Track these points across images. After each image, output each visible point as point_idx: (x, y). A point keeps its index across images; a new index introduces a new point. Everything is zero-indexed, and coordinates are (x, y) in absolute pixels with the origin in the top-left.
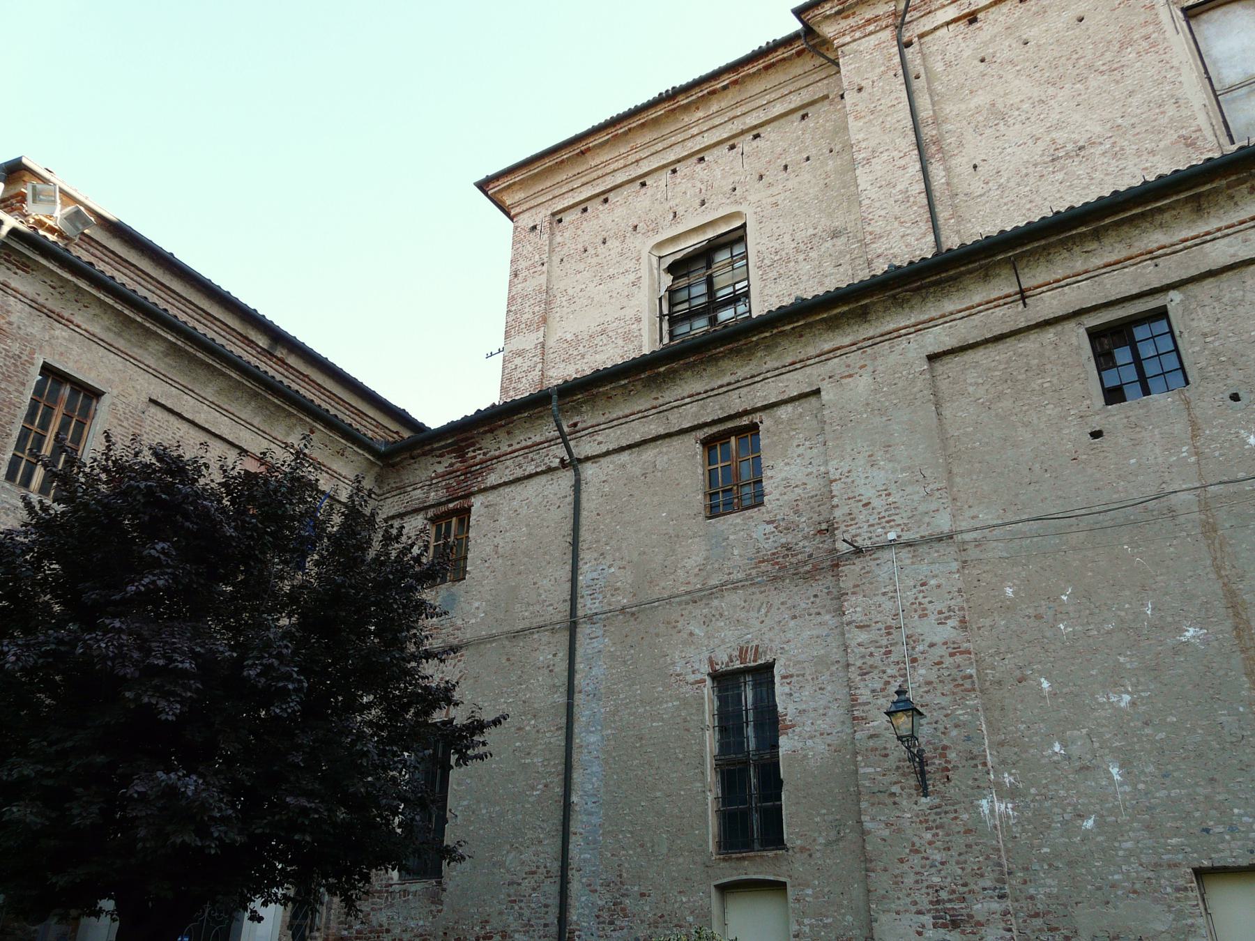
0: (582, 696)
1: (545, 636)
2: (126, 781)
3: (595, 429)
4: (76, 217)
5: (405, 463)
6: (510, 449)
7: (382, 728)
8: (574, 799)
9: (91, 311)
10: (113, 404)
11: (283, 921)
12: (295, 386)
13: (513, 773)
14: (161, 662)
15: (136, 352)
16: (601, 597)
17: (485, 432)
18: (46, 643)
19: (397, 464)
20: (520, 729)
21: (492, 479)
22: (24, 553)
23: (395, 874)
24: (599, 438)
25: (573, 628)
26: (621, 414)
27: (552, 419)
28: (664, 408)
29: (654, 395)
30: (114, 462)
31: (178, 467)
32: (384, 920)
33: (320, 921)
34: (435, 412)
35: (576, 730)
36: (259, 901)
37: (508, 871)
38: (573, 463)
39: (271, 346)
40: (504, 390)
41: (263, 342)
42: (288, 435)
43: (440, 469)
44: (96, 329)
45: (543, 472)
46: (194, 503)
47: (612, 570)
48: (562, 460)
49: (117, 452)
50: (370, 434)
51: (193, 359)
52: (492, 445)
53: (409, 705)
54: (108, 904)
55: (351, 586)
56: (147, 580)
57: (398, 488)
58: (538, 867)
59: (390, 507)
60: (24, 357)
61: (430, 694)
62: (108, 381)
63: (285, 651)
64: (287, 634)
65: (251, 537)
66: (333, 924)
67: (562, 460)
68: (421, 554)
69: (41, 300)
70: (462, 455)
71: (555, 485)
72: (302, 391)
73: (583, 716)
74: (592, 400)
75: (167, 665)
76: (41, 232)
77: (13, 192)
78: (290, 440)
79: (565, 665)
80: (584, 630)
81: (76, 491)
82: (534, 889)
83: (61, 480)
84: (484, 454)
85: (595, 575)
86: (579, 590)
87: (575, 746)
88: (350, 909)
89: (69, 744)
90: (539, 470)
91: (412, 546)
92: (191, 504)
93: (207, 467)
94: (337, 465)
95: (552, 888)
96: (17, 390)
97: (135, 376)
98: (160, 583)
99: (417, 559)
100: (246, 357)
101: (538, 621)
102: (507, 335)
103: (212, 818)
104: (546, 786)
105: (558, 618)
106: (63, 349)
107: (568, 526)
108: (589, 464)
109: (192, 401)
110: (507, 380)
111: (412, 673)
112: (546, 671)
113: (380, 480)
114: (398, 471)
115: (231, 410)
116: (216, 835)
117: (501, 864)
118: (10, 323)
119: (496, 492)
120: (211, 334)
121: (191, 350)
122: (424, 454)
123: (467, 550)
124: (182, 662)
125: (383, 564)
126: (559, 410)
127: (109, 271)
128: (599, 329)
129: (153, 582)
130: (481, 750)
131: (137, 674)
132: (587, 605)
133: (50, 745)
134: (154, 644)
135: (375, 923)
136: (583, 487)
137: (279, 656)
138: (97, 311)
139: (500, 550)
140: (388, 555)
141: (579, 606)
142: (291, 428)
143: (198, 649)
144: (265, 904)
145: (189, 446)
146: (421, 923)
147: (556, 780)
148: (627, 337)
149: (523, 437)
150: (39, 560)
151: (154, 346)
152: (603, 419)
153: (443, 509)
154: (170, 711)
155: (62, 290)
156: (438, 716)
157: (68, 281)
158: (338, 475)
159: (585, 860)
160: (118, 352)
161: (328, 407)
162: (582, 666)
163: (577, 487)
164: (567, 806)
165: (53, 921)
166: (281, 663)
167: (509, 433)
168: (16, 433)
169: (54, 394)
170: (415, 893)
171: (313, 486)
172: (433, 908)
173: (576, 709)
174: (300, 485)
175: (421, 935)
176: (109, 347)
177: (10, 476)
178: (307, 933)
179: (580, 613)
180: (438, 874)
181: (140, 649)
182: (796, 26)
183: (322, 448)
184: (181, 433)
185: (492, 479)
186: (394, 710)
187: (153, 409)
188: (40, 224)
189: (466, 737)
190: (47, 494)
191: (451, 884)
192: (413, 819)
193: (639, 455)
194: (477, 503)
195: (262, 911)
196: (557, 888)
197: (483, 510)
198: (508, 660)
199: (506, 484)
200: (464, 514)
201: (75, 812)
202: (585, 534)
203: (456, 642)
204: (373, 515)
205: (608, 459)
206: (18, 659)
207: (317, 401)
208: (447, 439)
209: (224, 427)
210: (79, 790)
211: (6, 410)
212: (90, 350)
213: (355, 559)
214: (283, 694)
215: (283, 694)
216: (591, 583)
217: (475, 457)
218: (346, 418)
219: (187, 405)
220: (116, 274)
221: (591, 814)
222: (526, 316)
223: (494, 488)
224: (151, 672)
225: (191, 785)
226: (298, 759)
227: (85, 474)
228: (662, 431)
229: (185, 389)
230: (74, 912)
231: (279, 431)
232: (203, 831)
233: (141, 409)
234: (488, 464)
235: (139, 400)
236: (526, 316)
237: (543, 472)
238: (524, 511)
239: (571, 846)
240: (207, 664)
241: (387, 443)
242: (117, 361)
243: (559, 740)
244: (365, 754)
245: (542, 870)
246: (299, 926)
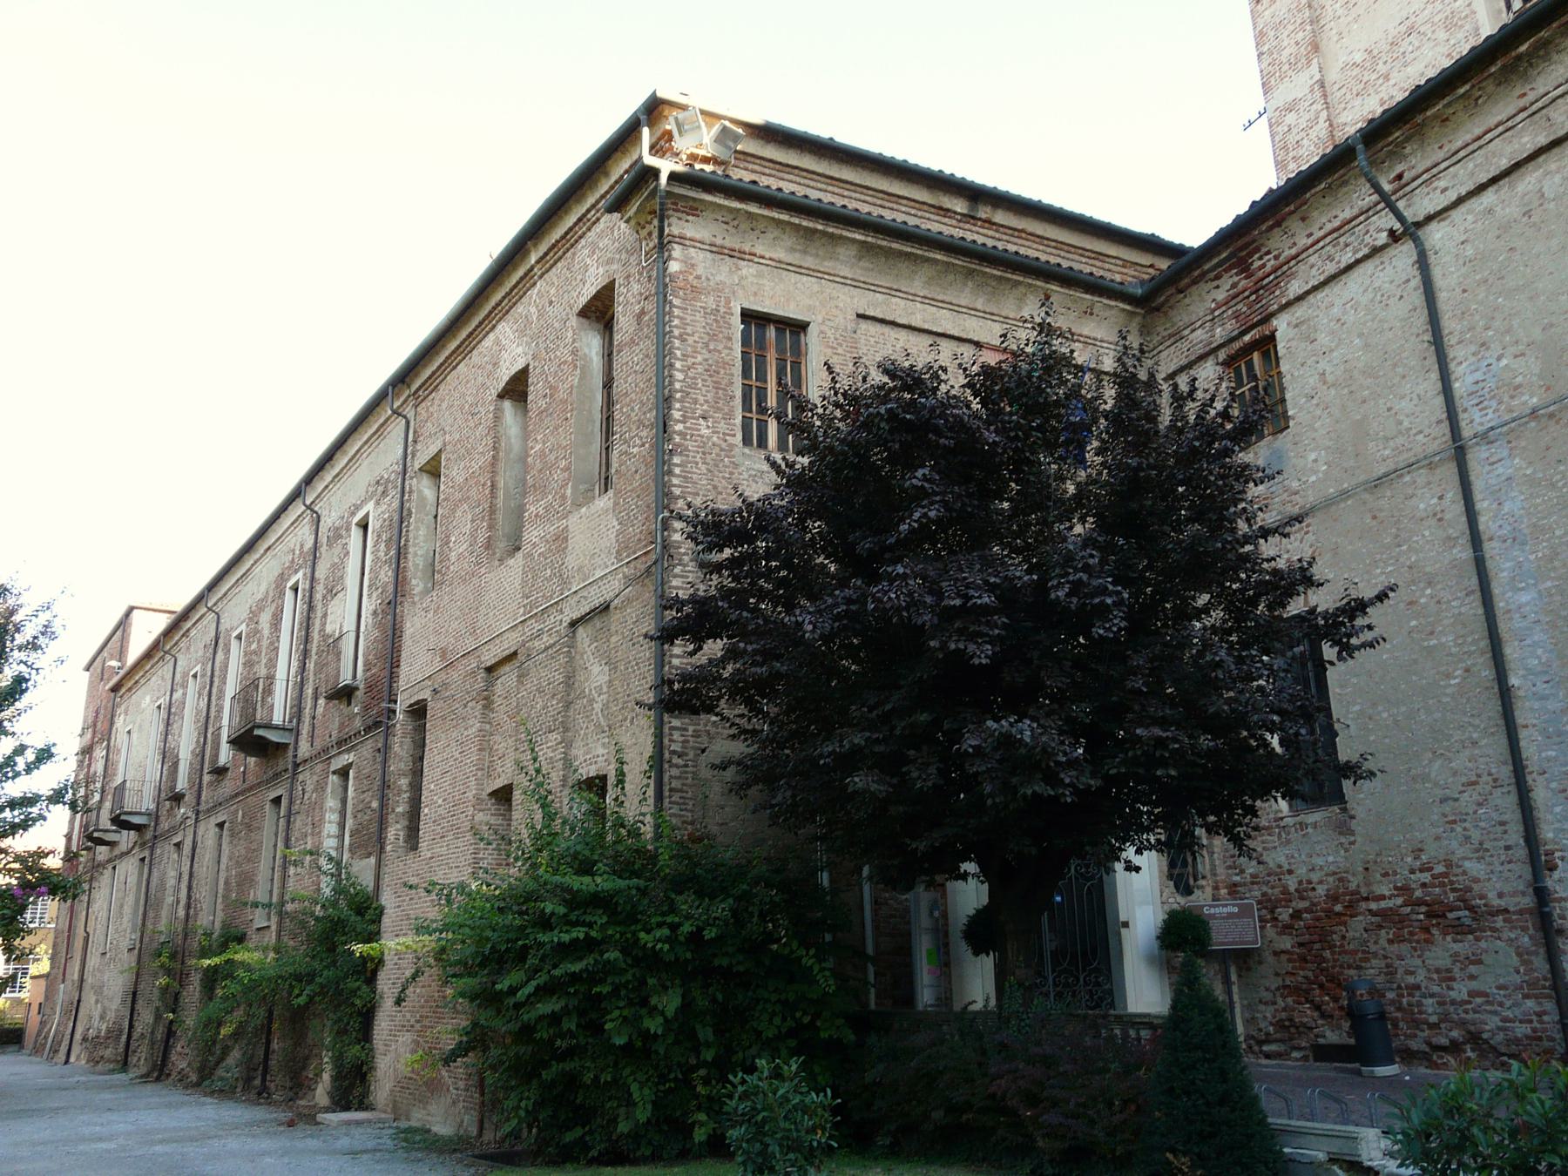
0: (1494, 544)
1: (1422, 476)
2: (955, 736)
3: (1432, 173)
4: (724, 136)
5: (1172, 301)
6: (1310, 241)
7: (1229, 632)
8: (1514, 681)
9: (770, 236)
11: (1161, 871)
12: (1012, 248)
13: (1415, 661)
14: (958, 602)
15: (828, 265)
16: (1494, 404)
17: (1271, 228)
18: (836, 605)
19: (1163, 304)
20: (1411, 603)
21: (1295, 288)
22: (786, 517)
23: (1283, 805)
24: (1442, 184)
25: (1460, 454)
26: (1468, 137)
27: (1363, 180)
28: (1539, 104)
29: (1518, 92)
30: (845, 395)
31: (914, 379)
32: (1282, 860)
33: (1204, 865)
34: (1192, 229)
35: (1496, 590)
36: (1132, 850)
37: (1436, 784)
38: (1409, 232)
39: (972, 208)
40: (1280, 165)
41: (960, 206)
42: (1020, 308)
43: (1221, 295)
44: (780, 254)
45: (1366, 257)
46: (943, 415)
47: (1504, 362)
48: (1392, 233)
49: (844, 383)
50: (1118, 278)
51: (889, 253)
52: (1281, 244)
53: (1257, 596)
54: (970, 867)
55: (1150, 467)
56: (917, 515)
57: (1170, 336)
58: (1479, 776)
59: (1169, 361)
60: (722, 310)
61: (1282, 578)
62: (810, 308)
63: (1091, 561)
64: (1088, 542)
65: (1017, 437)
66: (1220, 870)
67: (1392, 233)
68: (1228, 407)
69: (719, 241)
70: (1244, 267)
71: (1389, 269)
72: (1022, 251)
73: (1502, 569)
74: (1419, 133)
75: (964, 604)
76: (698, 166)
77: (658, 134)
78: (1026, 314)
79: (1460, 507)
80: (1477, 457)
81: (816, 436)
82: (1480, 804)
83: (795, 428)
84: (1276, 258)
85: (1478, 376)
86: (1458, 402)
87: (1499, 613)
88: (1240, 849)
89: (888, 707)
90: (1359, 255)
91: (1212, 400)
92: (940, 417)
93: (945, 370)
94: (1088, 328)
95: (1507, 802)
96: (726, 347)
97: (835, 294)
98: (932, 514)
99: (1225, 414)
100: (947, 231)
101: (1407, 457)
102: (1266, 88)
103: (1058, 763)
104: (1467, 670)
105: (1434, 446)
106: (754, 289)
107: (1422, 318)
108: (1434, 225)
109: (902, 303)
110: (1281, 150)
111: (1251, 561)
112: (1433, 522)
113: (1145, 330)
114: (1166, 314)
115: (948, 299)
116: (1067, 781)
117: (1425, 778)
118: (698, 277)
119: (1304, 304)
120: (900, 218)
121: (884, 243)
122: (1195, 282)
123: (1283, 390)
124: (980, 597)
125: (1181, 431)
126: (1372, 163)
127: (774, 184)
128: (1403, 28)
129: (925, 515)
130: (1368, 636)
131: (936, 621)
132: (1474, 421)
133: (870, 711)
134: (944, 584)
135: (1271, 865)
136: (1432, 259)
137: (1086, 568)
138: (776, 233)
139: (1330, 378)
140: (1184, 418)
141: (1463, 424)
142: (1021, 300)
143: (992, 580)
144: (1139, 852)
145: (919, 354)
146: (1331, 859)
147: (1481, 660)
148: (1450, 24)
149: (1325, 218)
150: (802, 520)
151: (845, 252)
152: (1441, 155)
153: (1237, 345)
154: (982, 654)
156: (1296, 607)
158: (1095, 339)
159: (1549, 759)
161: (1059, 260)
162: (1485, 504)
163: (1423, 263)
164: (1505, 694)
165: (921, 888)
166: (1090, 576)
167: (1303, 219)
168: (738, 393)
169: (762, 344)
170: (1315, 825)
171: (1066, 361)
172: (1343, 840)
173: (1489, 564)
174: (1054, 364)
175: (1335, 873)
176: (799, 270)
177: (747, 441)
178: (1191, 882)
179: (1467, 432)
180: (1339, 798)
181: (931, 592)
183: (1067, 312)
184: (901, 344)
185: (1295, 288)
186: (1239, 608)
187: (864, 326)
188: (693, 157)
189: (1343, 623)
190: (787, 450)
191: (1360, 809)
192: (1297, 734)
193: (1512, 187)
194: (1282, 326)
195: (1137, 860)
196: (1513, 799)
197: (1292, 333)
198: (1375, 517)
199: (1315, 289)
200: (1267, 344)
201: (915, 774)
202: (1449, 324)
203: (1296, 511)
204: (1152, 375)
205: (1463, 208)
206: (815, 627)
207: (1043, 258)
208: (1219, 253)
209: (945, 321)
210: (912, 752)
213: (1147, 432)
214: (1103, 612)
215: (1103, 612)
216: (1475, 388)
217: (1264, 266)
218: (1083, 266)
219: (897, 309)
220: (782, 184)
221: (1544, 698)
222: (1285, 53)
223: (1300, 298)
224: (948, 615)
225: (1026, 730)
226: (1138, 683)
227: (819, 416)
228: (1543, 140)
229: (891, 291)
230: (939, 878)
231: (1009, 308)
232: (1052, 779)
233: (863, 328)
234: (1283, 270)
235: (846, 319)
236: (1285, 53)
237: (1366, 257)
238: (1350, 317)
239: (1522, 744)
240: (1008, 595)
241: (1142, 282)
243: (1474, 608)
244: (1219, 665)
245: (1485, 778)
246: (1180, 875)
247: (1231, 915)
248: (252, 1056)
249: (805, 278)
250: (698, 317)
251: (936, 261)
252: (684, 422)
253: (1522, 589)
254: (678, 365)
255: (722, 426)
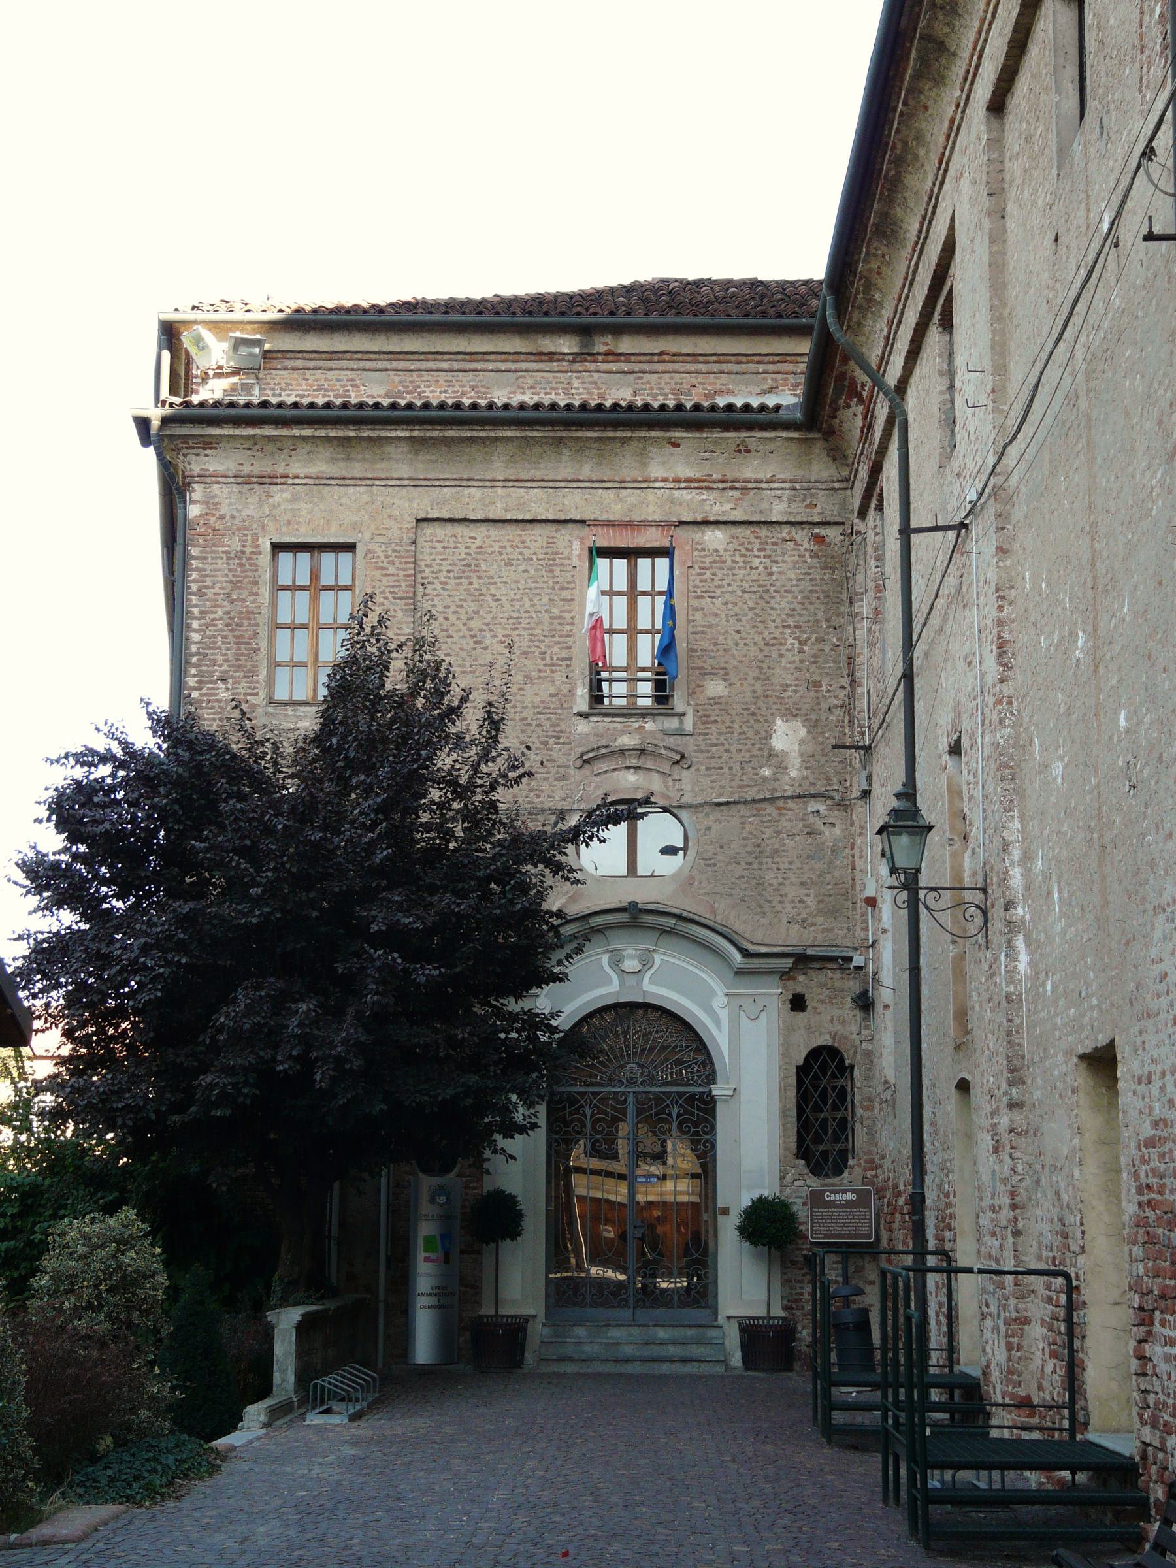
10: (369, 552)
15: (380, 469)
42: (645, 465)
60: (248, 550)
69: (246, 469)
98: (183, 961)
106: (289, 516)
118: (222, 517)
155: (258, 447)
157: (254, 436)
160: (357, 481)
176: (343, 481)
182: (151, 450)
184: (478, 542)
187: (429, 530)
211: (246, 623)
212: (322, 498)
219: (473, 501)
229: (460, 482)
242: (358, 494)
247: (850, 1203)
248: (120, 1093)
249: (352, 489)
250: (220, 564)
251: (508, 439)
252: (199, 689)
253: (609, 1294)
254: (195, 624)
255: (244, 687)
